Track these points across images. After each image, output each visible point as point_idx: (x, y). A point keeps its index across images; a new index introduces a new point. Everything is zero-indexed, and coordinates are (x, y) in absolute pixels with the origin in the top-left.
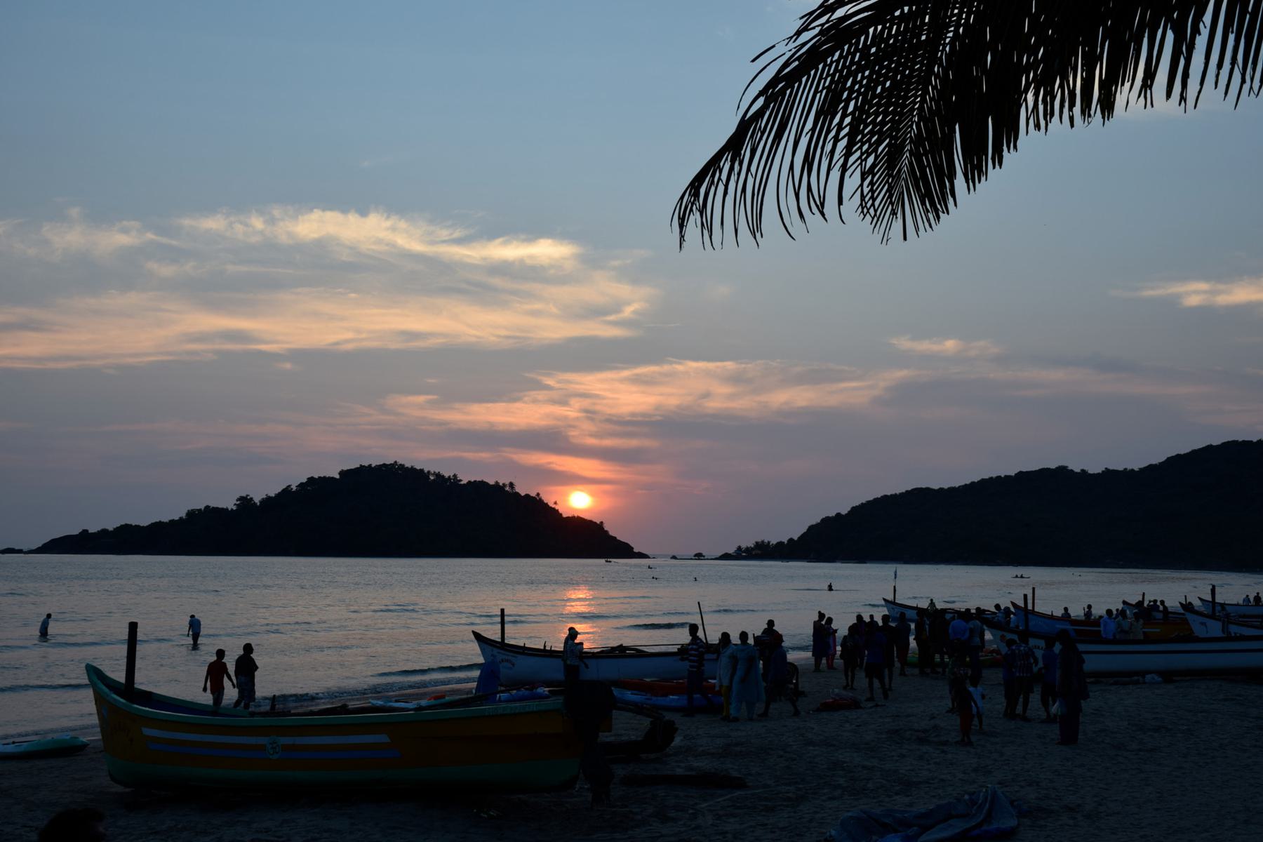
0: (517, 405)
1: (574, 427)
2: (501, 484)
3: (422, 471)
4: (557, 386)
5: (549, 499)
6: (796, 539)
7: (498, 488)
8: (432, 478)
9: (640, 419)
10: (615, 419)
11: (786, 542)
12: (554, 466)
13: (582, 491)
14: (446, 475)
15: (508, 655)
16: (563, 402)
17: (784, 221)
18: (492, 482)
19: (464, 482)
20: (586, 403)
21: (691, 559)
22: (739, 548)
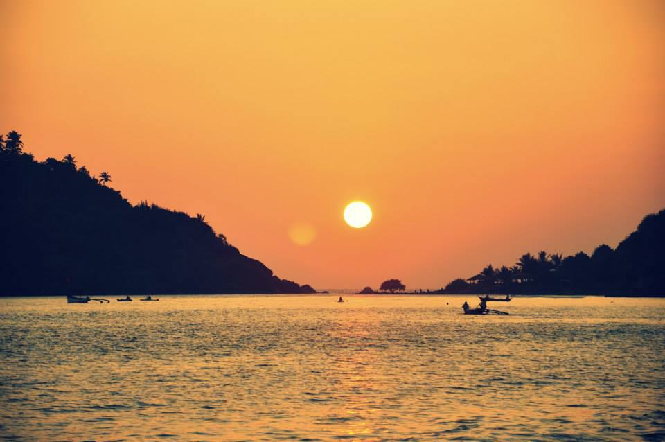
6: (614, 246)
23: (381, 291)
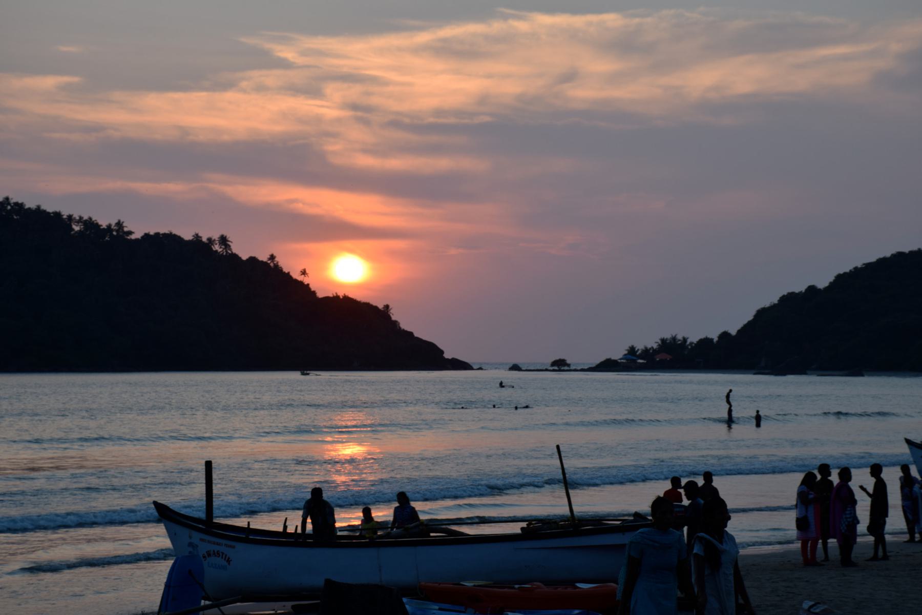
0: (230, 95)
1: (334, 135)
2: (204, 239)
3: (58, 215)
4: (300, 60)
5: (291, 266)
6: (733, 332)
7: (199, 246)
8: (76, 228)
9: (452, 120)
10: (407, 120)
11: (716, 339)
12: (300, 206)
13: (351, 251)
14: (104, 223)
15: (218, 544)
16: (312, 90)
17: (756, 513)
18: (187, 236)
19: (137, 235)
20: (354, 92)
21: (547, 370)
22: (632, 350)
23: (551, 368)
